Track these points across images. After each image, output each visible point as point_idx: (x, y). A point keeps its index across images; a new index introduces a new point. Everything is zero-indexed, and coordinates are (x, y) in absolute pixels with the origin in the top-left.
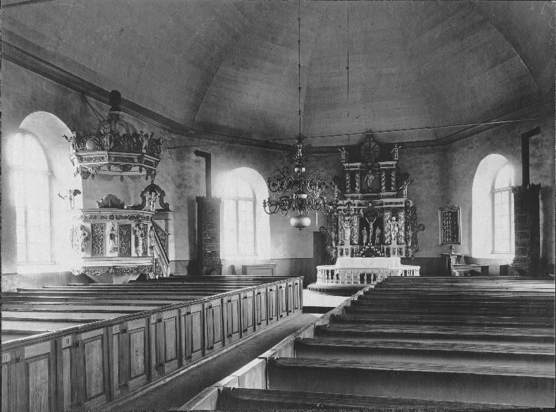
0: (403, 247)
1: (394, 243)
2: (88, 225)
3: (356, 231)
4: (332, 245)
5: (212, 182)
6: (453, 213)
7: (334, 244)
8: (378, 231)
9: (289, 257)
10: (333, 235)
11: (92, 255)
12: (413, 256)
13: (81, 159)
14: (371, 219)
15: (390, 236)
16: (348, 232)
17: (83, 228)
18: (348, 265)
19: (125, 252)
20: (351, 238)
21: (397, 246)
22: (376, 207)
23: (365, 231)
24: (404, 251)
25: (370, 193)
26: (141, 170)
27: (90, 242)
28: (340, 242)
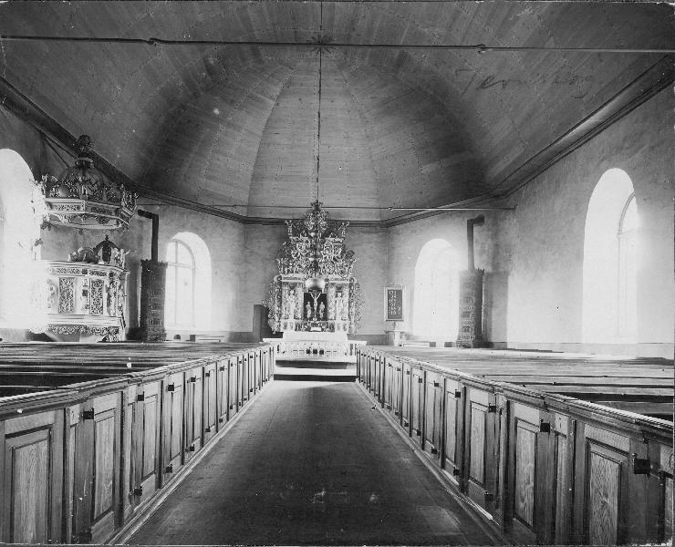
0: (347, 322)
1: (338, 318)
2: (56, 280)
3: (301, 306)
6: (397, 291)
8: (322, 306)
9: (228, 330)
12: (356, 332)
13: (50, 205)
15: (335, 311)
17: (50, 282)
18: (293, 342)
19: (96, 309)
20: (295, 312)
21: (342, 323)
24: (347, 327)
26: (118, 224)
28: (283, 316)
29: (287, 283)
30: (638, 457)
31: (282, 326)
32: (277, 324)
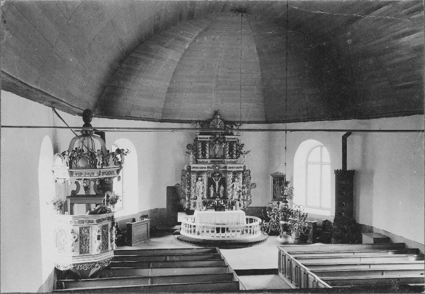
2: (77, 229)
4: (185, 198)
5: (253, 241)
7: (187, 199)
10: (186, 191)
11: (80, 253)
14: (217, 179)
16: (200, 187)
22: (221, 170)
23: (212, 188)
25: (217, 159)
27: (78, 242)
28: (193, 197)
29: (231, 171)
30: (373, 243)
31: (192, 205)
32: (187, 203)
